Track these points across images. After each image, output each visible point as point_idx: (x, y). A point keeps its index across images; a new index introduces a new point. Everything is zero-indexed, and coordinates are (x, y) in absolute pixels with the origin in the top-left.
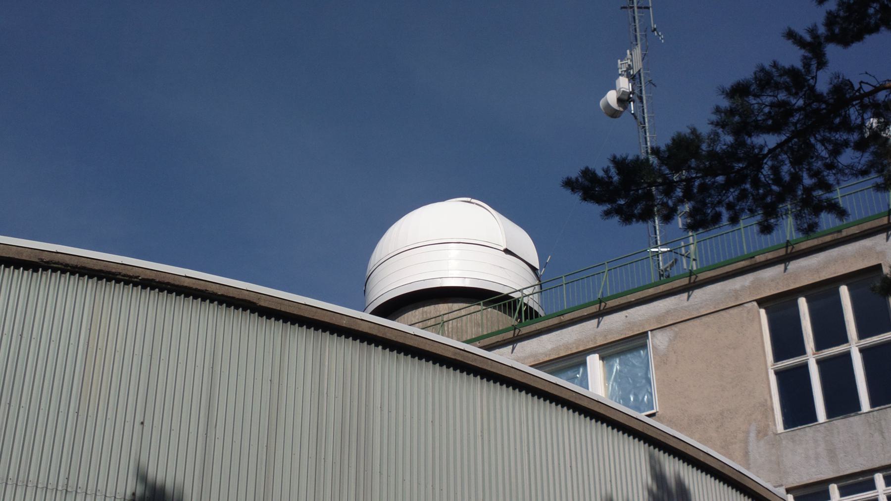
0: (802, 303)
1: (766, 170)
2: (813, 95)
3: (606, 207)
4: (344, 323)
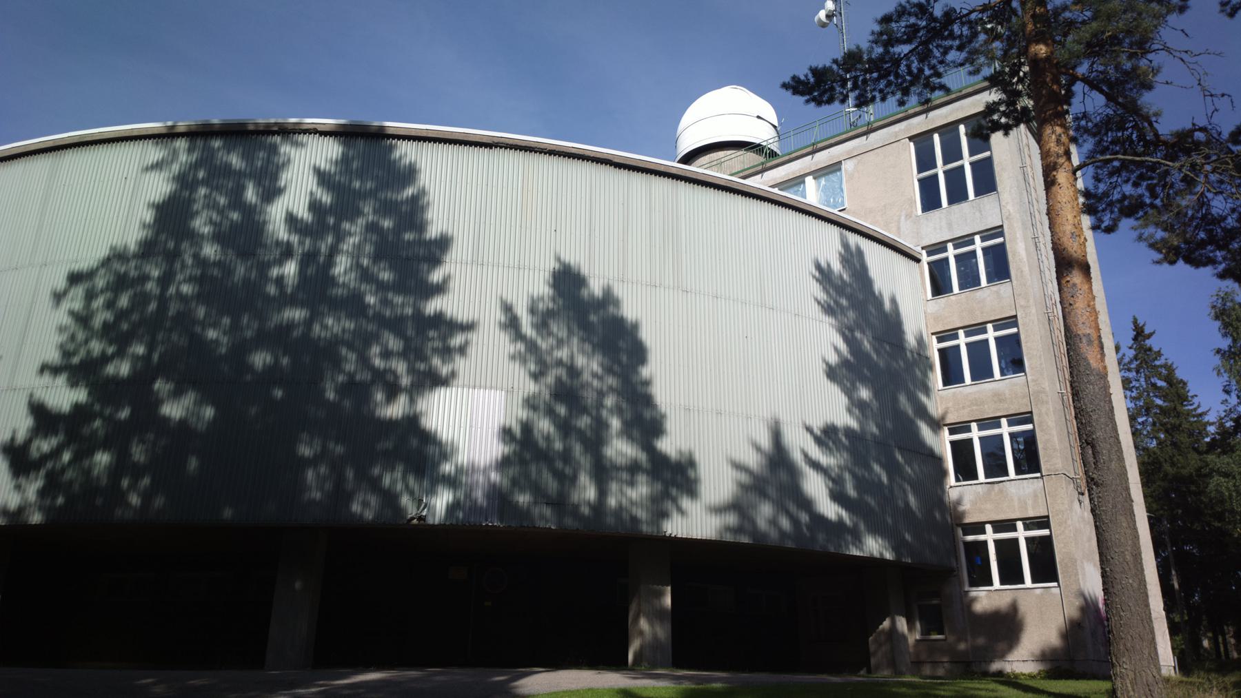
0: (936, 137)
1: (903, 67)
2: (933, 19)
3: (807, 97)
4: (662, 169)
